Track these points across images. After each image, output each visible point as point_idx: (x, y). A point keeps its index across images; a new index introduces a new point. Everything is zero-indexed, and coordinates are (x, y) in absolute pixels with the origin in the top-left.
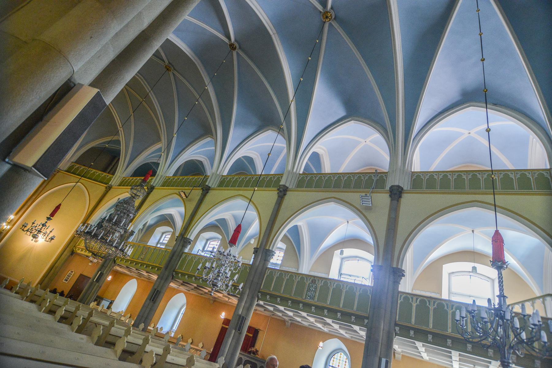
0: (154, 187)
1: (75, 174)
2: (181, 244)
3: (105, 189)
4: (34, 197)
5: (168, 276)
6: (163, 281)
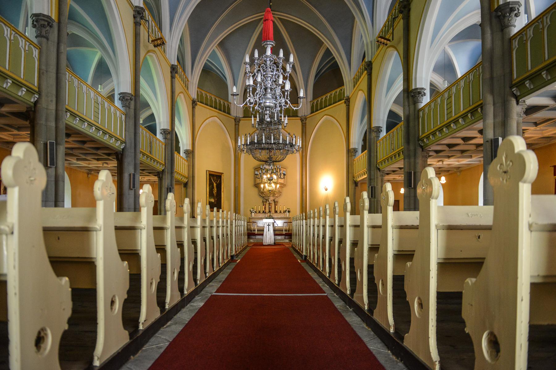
0: (370, 62)
1: (318, 110)
2: (411, 102)
3: (345, 105)
4: (304, 154)
5: (415, 150)
6: (412, 160)
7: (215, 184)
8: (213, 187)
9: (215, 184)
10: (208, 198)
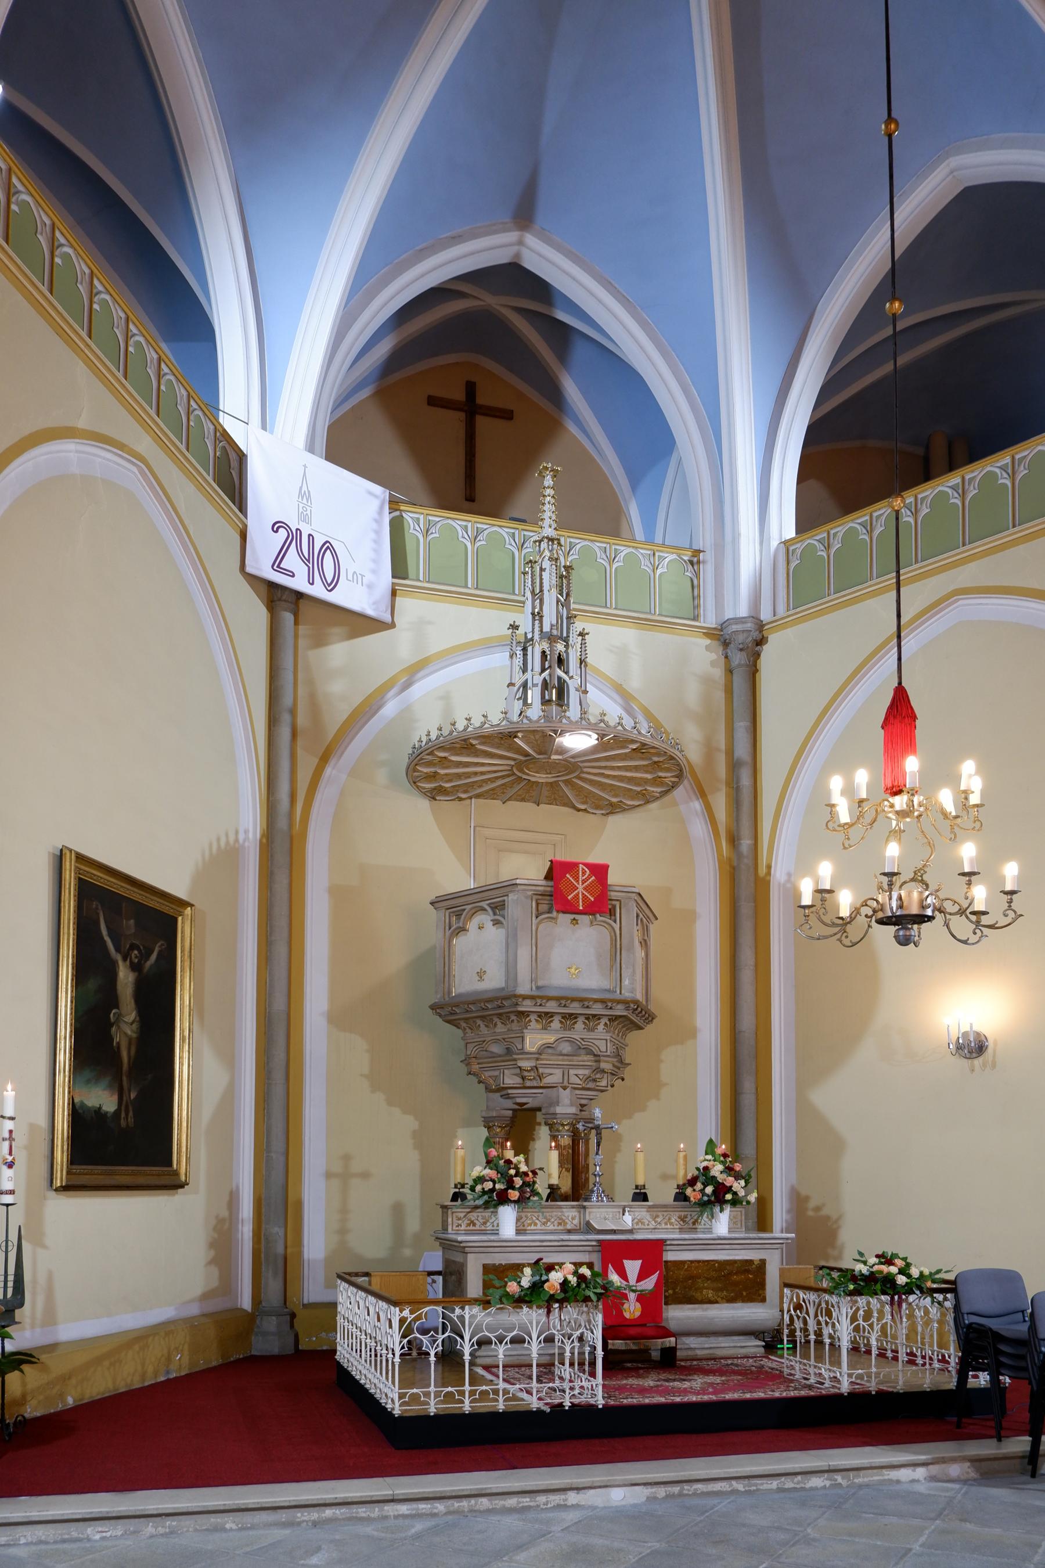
7: (125, 977)
8: (109, 997)
9: (125, 977)
10: (63, 1079)
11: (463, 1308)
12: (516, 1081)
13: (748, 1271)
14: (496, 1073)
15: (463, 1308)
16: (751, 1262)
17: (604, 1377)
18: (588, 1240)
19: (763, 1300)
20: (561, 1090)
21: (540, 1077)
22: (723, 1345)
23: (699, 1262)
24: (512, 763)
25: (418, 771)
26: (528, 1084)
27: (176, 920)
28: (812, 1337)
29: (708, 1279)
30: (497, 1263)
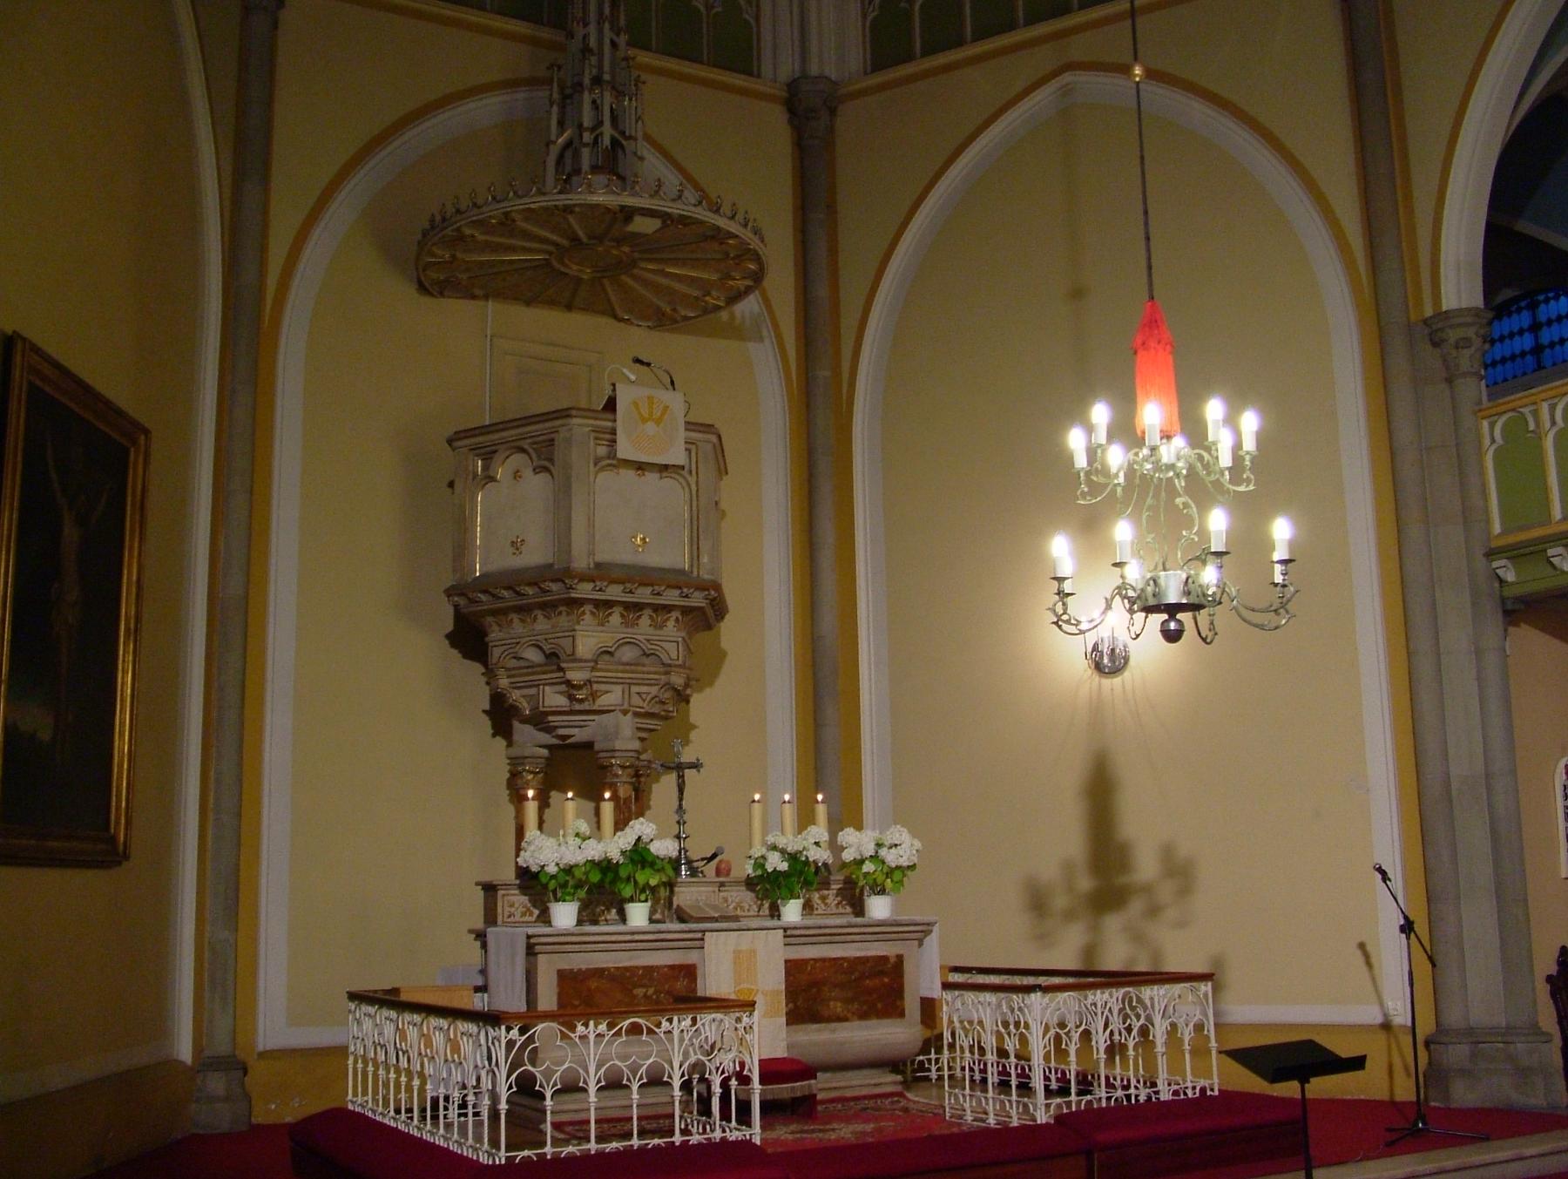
9: (70, 533)
11: (670, 1021)
12: (561, 701)
13: (882, 973)
14: (533, 691)
15: (670, 1021)
16: (885, 959)
17: (762, 1127)
18: (690, 931)
19: (902, 1014)
20: (620, 715)
21: (594, 696)
22: (854, 1083)
23: (824, 960)
24: (551, 248)
25: (434, 255)
26: (577, 707)
27: (127, 452)
28: (946, 1073)
29: (836, 986)
30: (575, 967)
